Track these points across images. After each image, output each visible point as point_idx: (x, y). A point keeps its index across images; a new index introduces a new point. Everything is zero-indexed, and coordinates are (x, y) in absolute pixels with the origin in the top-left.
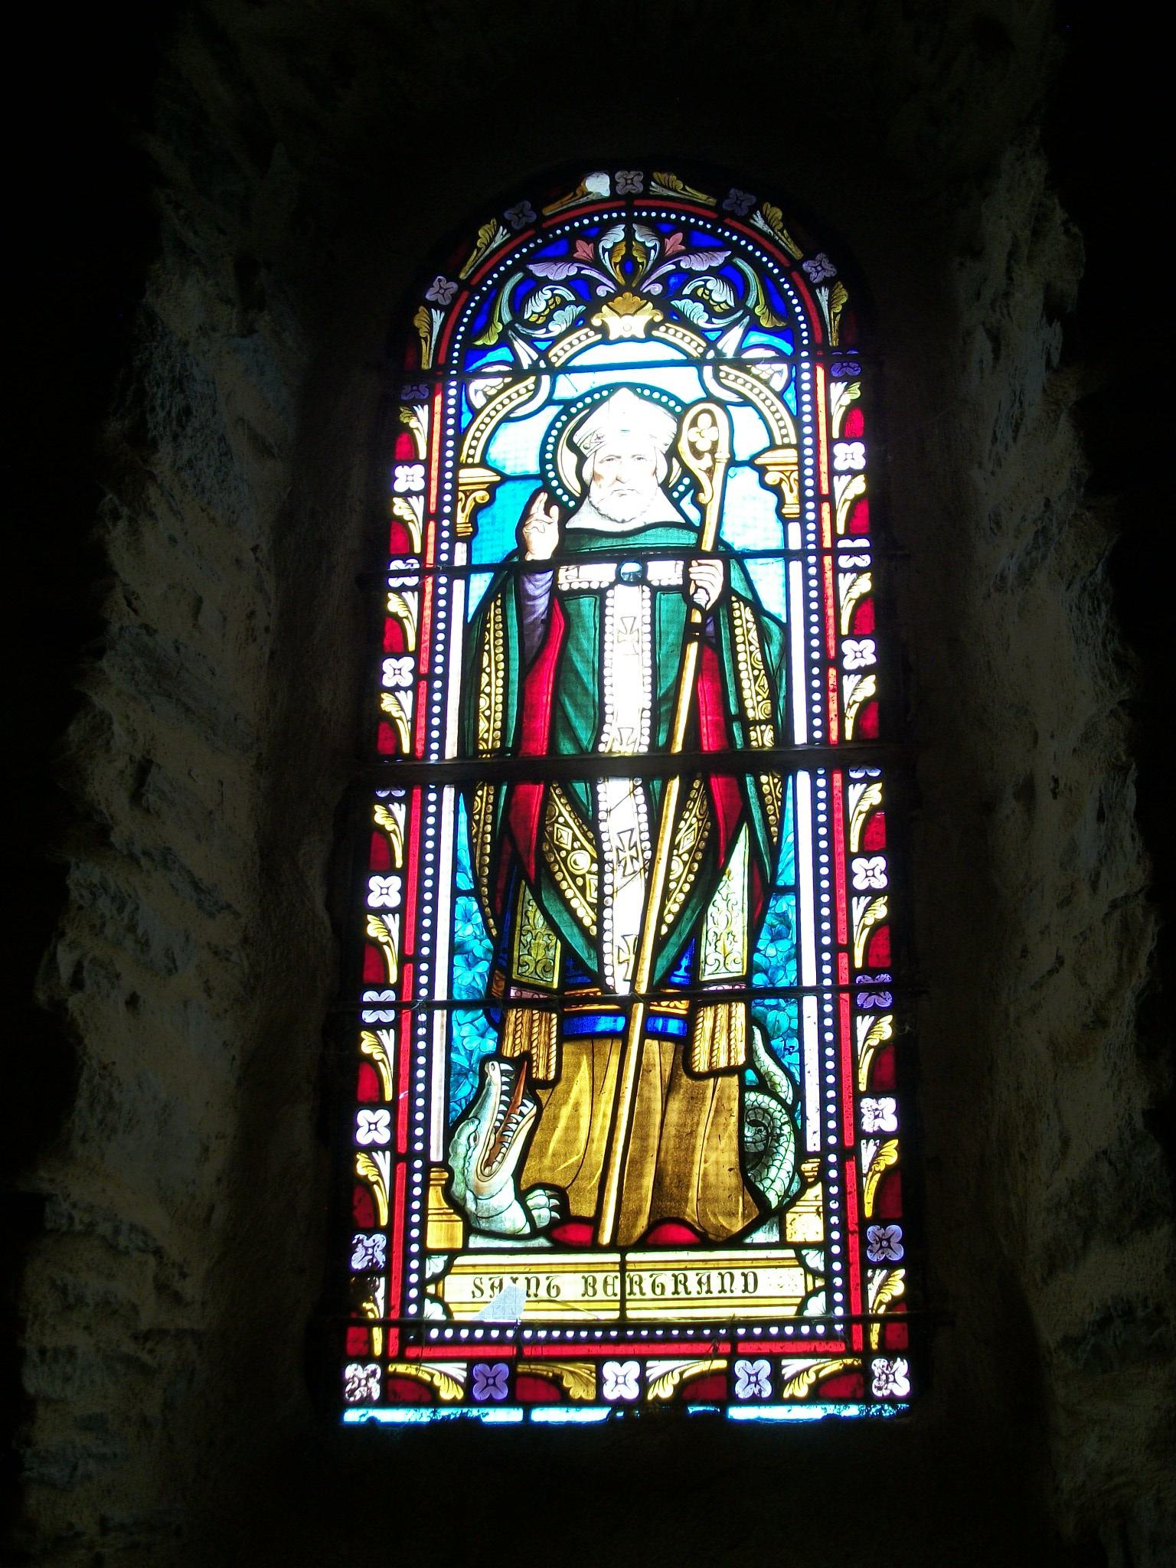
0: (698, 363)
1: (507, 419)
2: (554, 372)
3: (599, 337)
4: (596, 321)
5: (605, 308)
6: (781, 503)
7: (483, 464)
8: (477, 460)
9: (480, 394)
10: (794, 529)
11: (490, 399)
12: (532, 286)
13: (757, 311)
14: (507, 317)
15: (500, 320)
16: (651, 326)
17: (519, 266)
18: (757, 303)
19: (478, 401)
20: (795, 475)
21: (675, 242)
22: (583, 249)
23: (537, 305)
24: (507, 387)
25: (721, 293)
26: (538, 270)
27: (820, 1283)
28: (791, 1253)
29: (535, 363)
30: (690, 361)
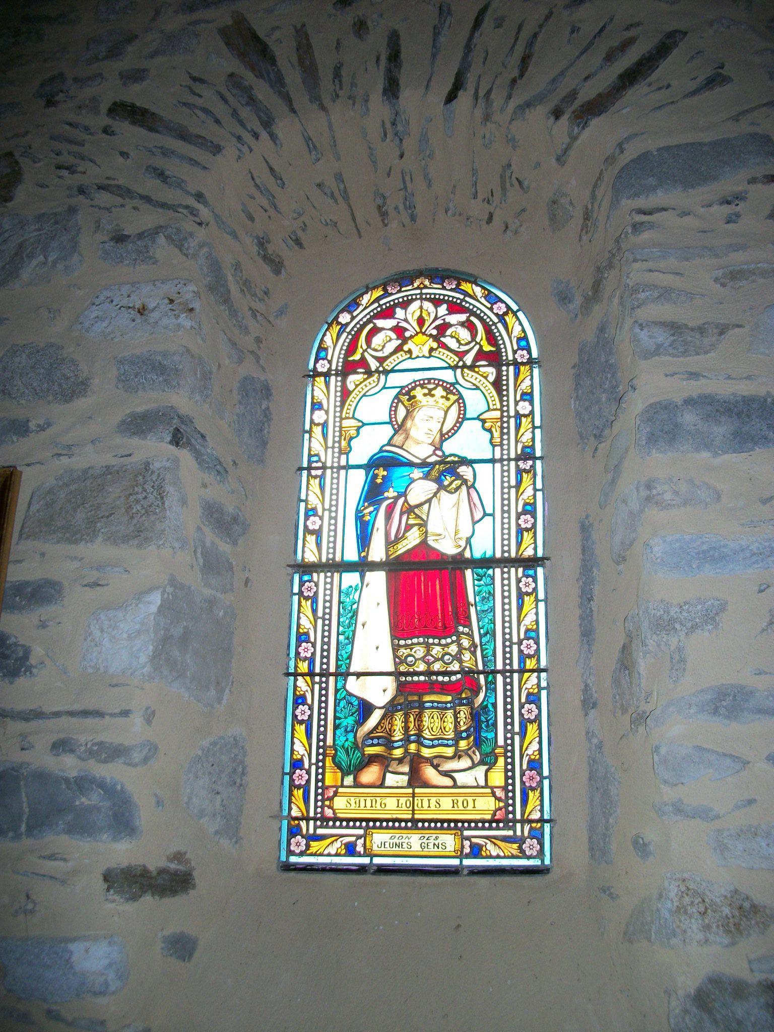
0: (454, 368)
1: (364, 395)
2: (386, 372)
3: (408, 356)
4: (406, 348)
5: (410, 342)
6: (492, 437)
7: (353, 417)
8: (351, 416)
9: (353, 383)
10: (498, 449)
11: (357, 386)
12: (375, 331)
13: (482, 343)
14: (365, 347)
15: (361, 347)
16: (432, 350)
17: (369, 321)
18: (482, 339)
19: (351, 387)
20: (499, 424)
21: (443, 309)
22: (400, 313)
23: (377, 340)
24: (365, 380)
25: (465, 334)
26: (380, 323)
27: (502, 804)
28: (489, 790)
29: (378, 368)
30: (450, 367)
